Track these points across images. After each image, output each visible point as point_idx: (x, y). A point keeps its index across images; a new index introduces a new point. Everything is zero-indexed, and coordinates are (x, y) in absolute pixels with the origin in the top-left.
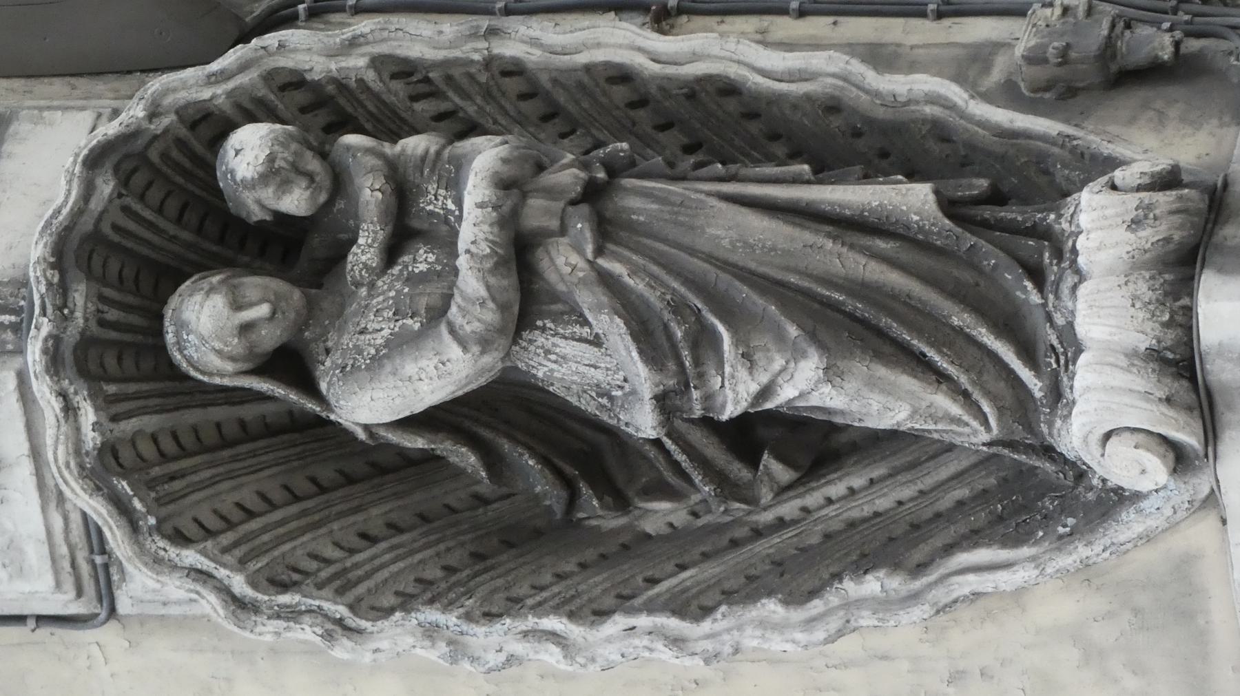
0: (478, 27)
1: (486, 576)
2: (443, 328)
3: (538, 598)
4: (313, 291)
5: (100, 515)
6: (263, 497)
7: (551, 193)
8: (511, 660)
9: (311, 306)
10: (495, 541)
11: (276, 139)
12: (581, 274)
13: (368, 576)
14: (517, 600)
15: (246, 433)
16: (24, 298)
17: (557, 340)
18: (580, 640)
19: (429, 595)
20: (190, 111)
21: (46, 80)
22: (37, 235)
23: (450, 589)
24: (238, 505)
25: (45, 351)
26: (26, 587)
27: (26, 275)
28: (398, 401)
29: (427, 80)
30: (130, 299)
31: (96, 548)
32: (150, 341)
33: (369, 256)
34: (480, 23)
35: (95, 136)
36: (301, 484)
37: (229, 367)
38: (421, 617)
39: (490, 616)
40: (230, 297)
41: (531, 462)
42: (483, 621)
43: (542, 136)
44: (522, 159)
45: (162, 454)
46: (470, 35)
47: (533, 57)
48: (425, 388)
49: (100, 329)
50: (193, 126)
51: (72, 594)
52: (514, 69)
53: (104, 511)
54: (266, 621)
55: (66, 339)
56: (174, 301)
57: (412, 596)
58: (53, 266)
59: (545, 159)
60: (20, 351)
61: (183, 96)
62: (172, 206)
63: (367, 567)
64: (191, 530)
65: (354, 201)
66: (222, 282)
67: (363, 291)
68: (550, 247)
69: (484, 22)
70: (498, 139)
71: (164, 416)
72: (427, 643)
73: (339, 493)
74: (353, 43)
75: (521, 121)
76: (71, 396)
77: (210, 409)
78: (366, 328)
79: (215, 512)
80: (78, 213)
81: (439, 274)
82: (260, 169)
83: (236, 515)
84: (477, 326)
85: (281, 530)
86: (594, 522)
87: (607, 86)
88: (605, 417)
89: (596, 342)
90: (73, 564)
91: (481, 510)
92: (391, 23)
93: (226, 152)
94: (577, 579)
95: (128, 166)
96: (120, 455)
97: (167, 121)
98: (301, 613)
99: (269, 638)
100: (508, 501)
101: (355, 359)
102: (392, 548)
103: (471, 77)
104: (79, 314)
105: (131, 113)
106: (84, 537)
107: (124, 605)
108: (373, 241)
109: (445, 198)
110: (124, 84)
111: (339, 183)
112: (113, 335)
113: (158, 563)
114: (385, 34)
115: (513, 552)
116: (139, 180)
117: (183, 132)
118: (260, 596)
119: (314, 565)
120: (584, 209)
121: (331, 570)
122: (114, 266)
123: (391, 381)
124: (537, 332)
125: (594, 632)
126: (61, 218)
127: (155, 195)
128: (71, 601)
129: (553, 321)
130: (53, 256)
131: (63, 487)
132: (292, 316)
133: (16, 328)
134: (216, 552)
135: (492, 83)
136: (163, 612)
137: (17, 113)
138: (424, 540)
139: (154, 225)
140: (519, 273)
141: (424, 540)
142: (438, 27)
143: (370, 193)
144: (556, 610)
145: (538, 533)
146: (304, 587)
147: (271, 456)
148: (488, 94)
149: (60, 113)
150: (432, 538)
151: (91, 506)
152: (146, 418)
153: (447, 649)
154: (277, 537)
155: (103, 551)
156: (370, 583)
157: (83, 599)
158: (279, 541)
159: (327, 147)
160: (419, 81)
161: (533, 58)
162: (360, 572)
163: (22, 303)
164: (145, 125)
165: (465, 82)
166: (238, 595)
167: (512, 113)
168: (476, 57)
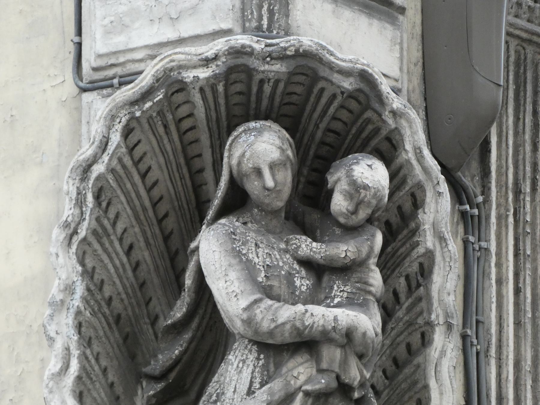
0: (453, 317)
1: (105, 324)
2: (258, 296)
3: (90, 357)
4: (283, 215)
5: (142, 81)
6: (155, 183)
7: (344, 363)
8: (51, 340)
9: (275, 213)
10: (128, 329)
11: (379, 190)
12: (292, 382)
13: (105, 250)
14: (89, 343)
15: (195, 174)
16: (278, 33)
17: (251, 367)
18: (64, 384)
19: (92, 288)
20: (397, 137)
21: (420, 47)
22: (317, 41)
23: (96, 301)
24: (150, 168)
25: (243, 46)
26: (98, 36)
27: (293, 34)
28: (213, 268)
29: (419, 285)
30: (277, 100)
31: (122, 79)
32: (252, 112)
33: (305, 249)
34: (455, 319)
35: (380, 77)
36: (163, 208)
37: (234, 162)
38: (78, 283)
39: (79, 326)
40: (279, 162)
41: (177, 352)
42: (76, 322)
43: (384, 358)
44: (365, 344)
45: (181, 120)
46: (447, 313)
47: (434, 352)
48: (221, 285)
49: (257, 81)
50: (388, 139)
51: (94, 65)
52: (426, 340)
53: (143, 84)
54: (75, 185)
55: (251, 59)
56: (276, 127)
57: (92, 278)
58: (297, 51)
59: (367, 359)
60: (244, 31)
61: (407, 132)
62: (337, 126)
63: (110, 249)
64: (133, 139)
65: (339, 240)
66: (288, 157)
67: (283, 246)
68: (310, 363)
69: (457, 321)
70: (379, 330)
71: (205, 122)
72: (62, 287)
73: (157, 231)
74: (442, 239)
75: (394, 345)
76: (215, 63)
77: (210, 150)
78: (259, 247)
79: (145, 154)
80: (331, 66)
81: (293, 293)
82: (359, 180)
83: (143, 167)
84: (259, 317)
85: (133, 195)
86: (140, 392)
87: (415, 399)
88: (204, 398)
89: (250, 392)
90: (113, 65)
91: (147, 321)
92: (454, 264)
93: (371, 159)
94: (103, 381)
95: (362, 98)
96: (179, 94)
97: (391, 121)
98: (81, 208)
99: (65, 187)
100: (153, 337)
101: (239, 241)
102: (123, 265)
103: (421, 313)
104: (267, 67)
105: (396, 100)
106: (129, 72)
107: (87, 97)
108: (314, 252)
109: (342, 297)
110: (418, 97)
111: (351, 230)
112: (255, 89)
113: (112, 118)
114: (448, 259)
115: (121, 341)
116: (353, 105)
117: (384, 133)
118: (91, 182)
119: (112, 215)
120: (334, 384)
121: (109, 227)
122: (299, 89)
123: (225, 263)
124: (256, 355)
125: (69, 392)
126: (327, 56)
127: (344, 115)
128: (90, 64)
129: (263, 365)
130: (303, 51)
131: (158, 58)
132: (267, 201)
133: (259, 28)
134: (119, 154)
135: (417, 326)
136: (84, 122)
137: (398, 29)
138: (128, 285)
139: (326, 117)
140: (293, 343)
141: (128, 285)
142: (452, 293)
143: (344, 250)
144: (83, 368)
145: (133, 357)
146: (97, 209)
147: (181, 189)
148: (410, 324)
149: (398, 55)
150: (130, 291)
151: (146, 76)
152: (203, 110)
153: (58, 300)
154: (129, 193)
155: (121, 84)
156: (100, 251)
157: (91, 71)
158: (126, 194)
159: (376, 223)
160: (418, 281)
161: (433, 352)
162: (107, 245)
163: (275, 32)
164: (388, 109)
165: (418, 309)
166: (92, 168)
167: (398, 339)
168: (433, 317)
